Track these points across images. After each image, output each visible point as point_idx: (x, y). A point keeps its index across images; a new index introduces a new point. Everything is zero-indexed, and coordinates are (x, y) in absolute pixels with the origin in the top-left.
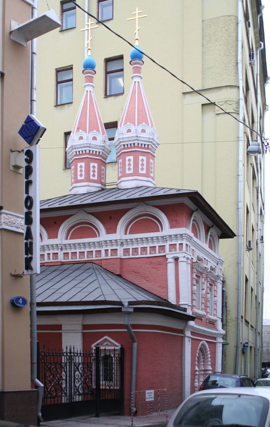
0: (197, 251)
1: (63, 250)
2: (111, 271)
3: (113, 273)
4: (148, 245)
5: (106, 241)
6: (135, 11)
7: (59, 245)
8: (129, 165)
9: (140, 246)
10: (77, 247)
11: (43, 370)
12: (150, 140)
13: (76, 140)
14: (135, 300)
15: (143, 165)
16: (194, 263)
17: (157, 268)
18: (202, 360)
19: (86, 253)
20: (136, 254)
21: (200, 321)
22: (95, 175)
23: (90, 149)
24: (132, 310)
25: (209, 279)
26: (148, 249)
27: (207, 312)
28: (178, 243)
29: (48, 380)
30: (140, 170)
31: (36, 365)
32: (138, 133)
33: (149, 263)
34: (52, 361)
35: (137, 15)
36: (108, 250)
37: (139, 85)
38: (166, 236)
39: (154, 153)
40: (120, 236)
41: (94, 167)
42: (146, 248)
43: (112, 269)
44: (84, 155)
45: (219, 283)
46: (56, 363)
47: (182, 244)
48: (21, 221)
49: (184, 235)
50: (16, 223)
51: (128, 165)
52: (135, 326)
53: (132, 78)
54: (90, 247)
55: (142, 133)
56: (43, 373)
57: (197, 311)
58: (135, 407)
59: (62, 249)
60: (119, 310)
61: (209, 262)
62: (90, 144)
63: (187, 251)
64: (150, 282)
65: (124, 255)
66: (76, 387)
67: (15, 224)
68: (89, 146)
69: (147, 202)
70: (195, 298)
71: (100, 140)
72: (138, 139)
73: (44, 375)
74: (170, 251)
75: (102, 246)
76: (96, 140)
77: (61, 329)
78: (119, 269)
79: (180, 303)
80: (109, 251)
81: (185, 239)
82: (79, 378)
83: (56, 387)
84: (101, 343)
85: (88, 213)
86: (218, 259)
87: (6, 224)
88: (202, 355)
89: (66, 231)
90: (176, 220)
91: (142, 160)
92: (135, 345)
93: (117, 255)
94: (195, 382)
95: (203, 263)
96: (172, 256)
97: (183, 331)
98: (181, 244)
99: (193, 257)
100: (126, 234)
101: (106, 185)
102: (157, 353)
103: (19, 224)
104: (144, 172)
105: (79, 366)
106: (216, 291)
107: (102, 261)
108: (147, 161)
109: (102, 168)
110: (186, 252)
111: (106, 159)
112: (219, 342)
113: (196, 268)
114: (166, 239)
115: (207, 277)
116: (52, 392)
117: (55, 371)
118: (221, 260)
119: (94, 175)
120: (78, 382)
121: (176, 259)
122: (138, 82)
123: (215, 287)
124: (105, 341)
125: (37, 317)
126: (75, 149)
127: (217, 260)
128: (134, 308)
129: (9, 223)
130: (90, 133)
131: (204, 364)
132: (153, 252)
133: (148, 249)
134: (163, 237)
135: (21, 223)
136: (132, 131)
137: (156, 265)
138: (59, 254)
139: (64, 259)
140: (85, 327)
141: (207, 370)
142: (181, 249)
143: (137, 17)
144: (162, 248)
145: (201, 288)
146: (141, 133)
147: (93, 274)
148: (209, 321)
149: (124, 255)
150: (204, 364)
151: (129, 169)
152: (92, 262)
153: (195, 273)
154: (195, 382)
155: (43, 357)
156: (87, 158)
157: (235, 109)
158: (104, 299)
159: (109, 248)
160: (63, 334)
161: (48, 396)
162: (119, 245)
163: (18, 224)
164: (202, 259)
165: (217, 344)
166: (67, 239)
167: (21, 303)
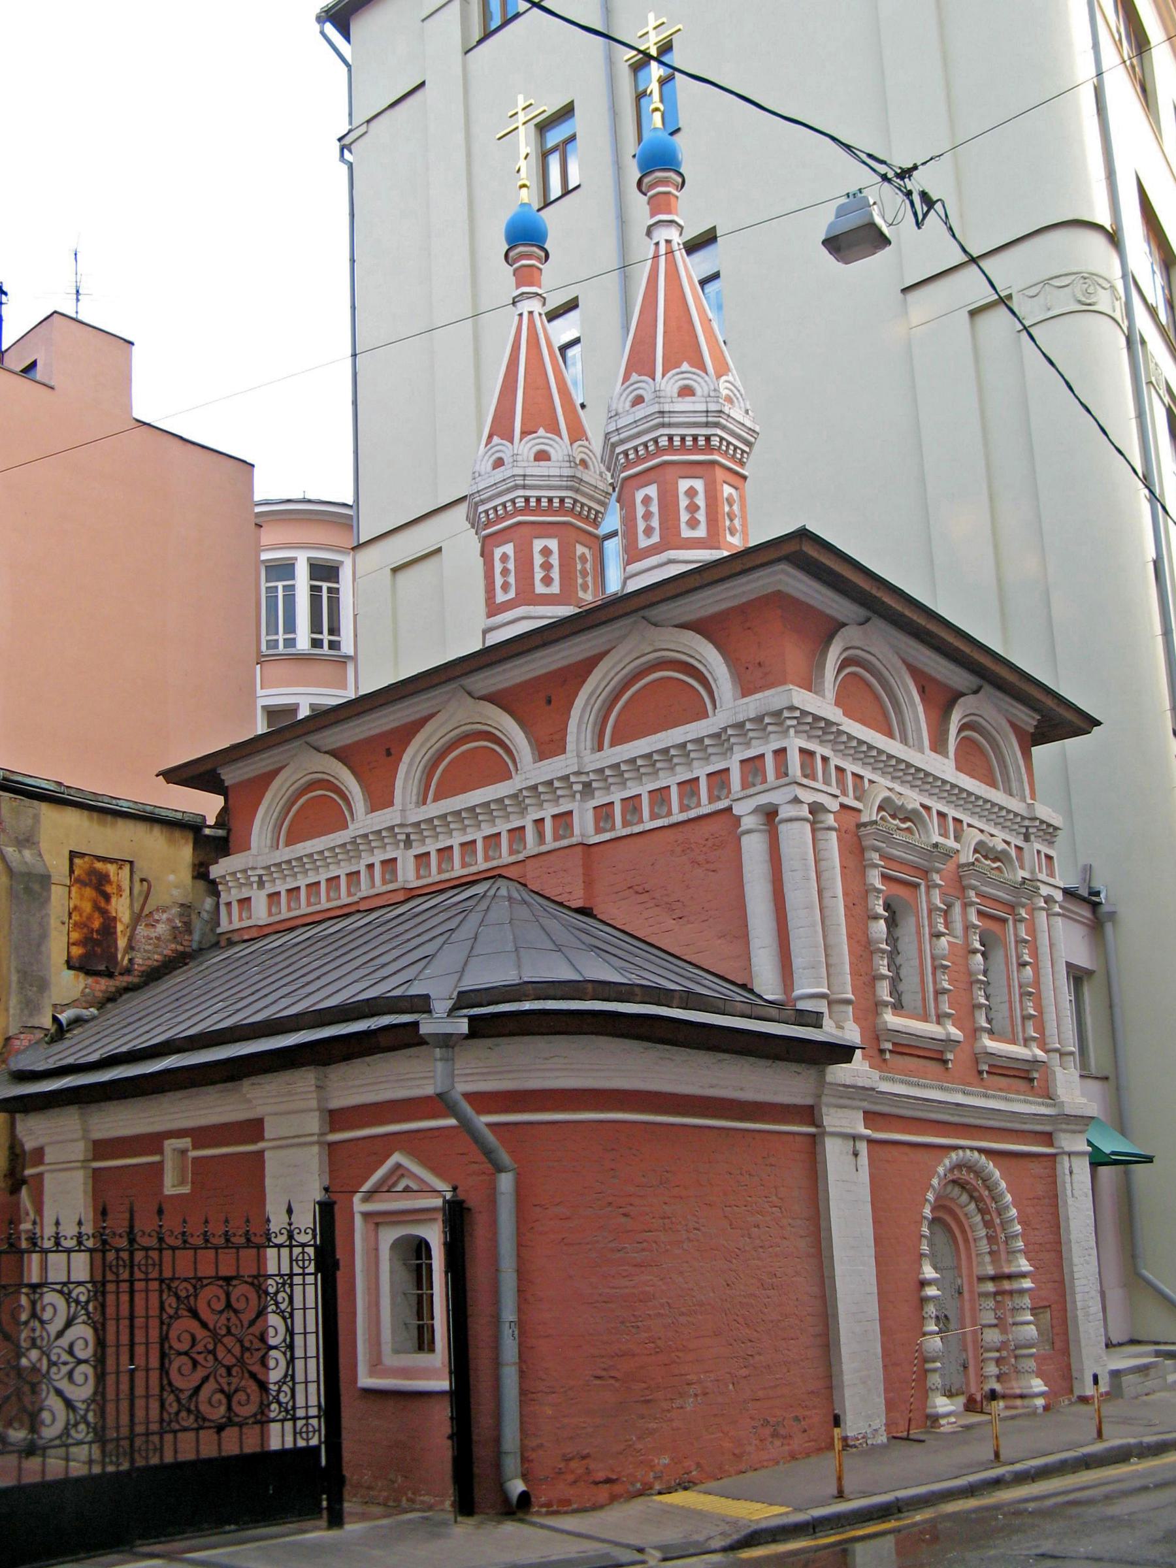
1: (414, 844)
2: (556, 899)
4: (670, 780)
5: (534, 788)
7: (397, 830)
9: (643, 789)
12: (710, 419)
13: (483, 473)
23: (528, 493)
24: (463, 1027)
25: (972, 893)
30: (683, 526)
32: (662, 400)
33: (678, 850)
35: (652, 34)
36: (542, 820)
38: (725, 729)
39: (741, 463)
40: (575, 760)
41: (546, 552)
43: (560, 890)
44: (512, 516)
47: (784, 750)
49: (786, 714)
52: (484, 1101)
53: (649, 233)
58: (525, 1477)
59: (408, 843)
61: (969, 825)
62: (524, 476)
64: (689, 922)
65: (599, 830)
66: (174, 1390)
68: (522, 482)
70: (946, 985)
72: (666, 420)
74: (744, 786)
76: (548, 459)
77: (260, 1137)
79: (798, 992)
80: (548, 824)
81: (792, 731)
86: (1023, 818)
91: (691, 492)
92: (506, 1182)
96: (752, 804)
98: (781, 753)
102: (625, 1215)
104: (701, 532)
108: (706, 491)
109: (578, 553)
111: (596, 523)
113: (876, 849)
119: (547, 581)
121: (770, 814)
124: (399, 1173)
128: (472, 1019)
130: (525, 439)
131: (995, 1248)
133: (674, 792)
136: (646, 399)
137: (704, 849)
139: (418, 877)
141: (1009, 1277)
142: (782, 771)
144: (719, 778)
145: (927, 929)
149: (599, 830)
152: (500, 876)
153: (876, 866)
156: (519, 524)
157: (1083, 299)
160: (267, 1155)
162: (578, 796)
164: (915, 811)
165: (1058, 1158)
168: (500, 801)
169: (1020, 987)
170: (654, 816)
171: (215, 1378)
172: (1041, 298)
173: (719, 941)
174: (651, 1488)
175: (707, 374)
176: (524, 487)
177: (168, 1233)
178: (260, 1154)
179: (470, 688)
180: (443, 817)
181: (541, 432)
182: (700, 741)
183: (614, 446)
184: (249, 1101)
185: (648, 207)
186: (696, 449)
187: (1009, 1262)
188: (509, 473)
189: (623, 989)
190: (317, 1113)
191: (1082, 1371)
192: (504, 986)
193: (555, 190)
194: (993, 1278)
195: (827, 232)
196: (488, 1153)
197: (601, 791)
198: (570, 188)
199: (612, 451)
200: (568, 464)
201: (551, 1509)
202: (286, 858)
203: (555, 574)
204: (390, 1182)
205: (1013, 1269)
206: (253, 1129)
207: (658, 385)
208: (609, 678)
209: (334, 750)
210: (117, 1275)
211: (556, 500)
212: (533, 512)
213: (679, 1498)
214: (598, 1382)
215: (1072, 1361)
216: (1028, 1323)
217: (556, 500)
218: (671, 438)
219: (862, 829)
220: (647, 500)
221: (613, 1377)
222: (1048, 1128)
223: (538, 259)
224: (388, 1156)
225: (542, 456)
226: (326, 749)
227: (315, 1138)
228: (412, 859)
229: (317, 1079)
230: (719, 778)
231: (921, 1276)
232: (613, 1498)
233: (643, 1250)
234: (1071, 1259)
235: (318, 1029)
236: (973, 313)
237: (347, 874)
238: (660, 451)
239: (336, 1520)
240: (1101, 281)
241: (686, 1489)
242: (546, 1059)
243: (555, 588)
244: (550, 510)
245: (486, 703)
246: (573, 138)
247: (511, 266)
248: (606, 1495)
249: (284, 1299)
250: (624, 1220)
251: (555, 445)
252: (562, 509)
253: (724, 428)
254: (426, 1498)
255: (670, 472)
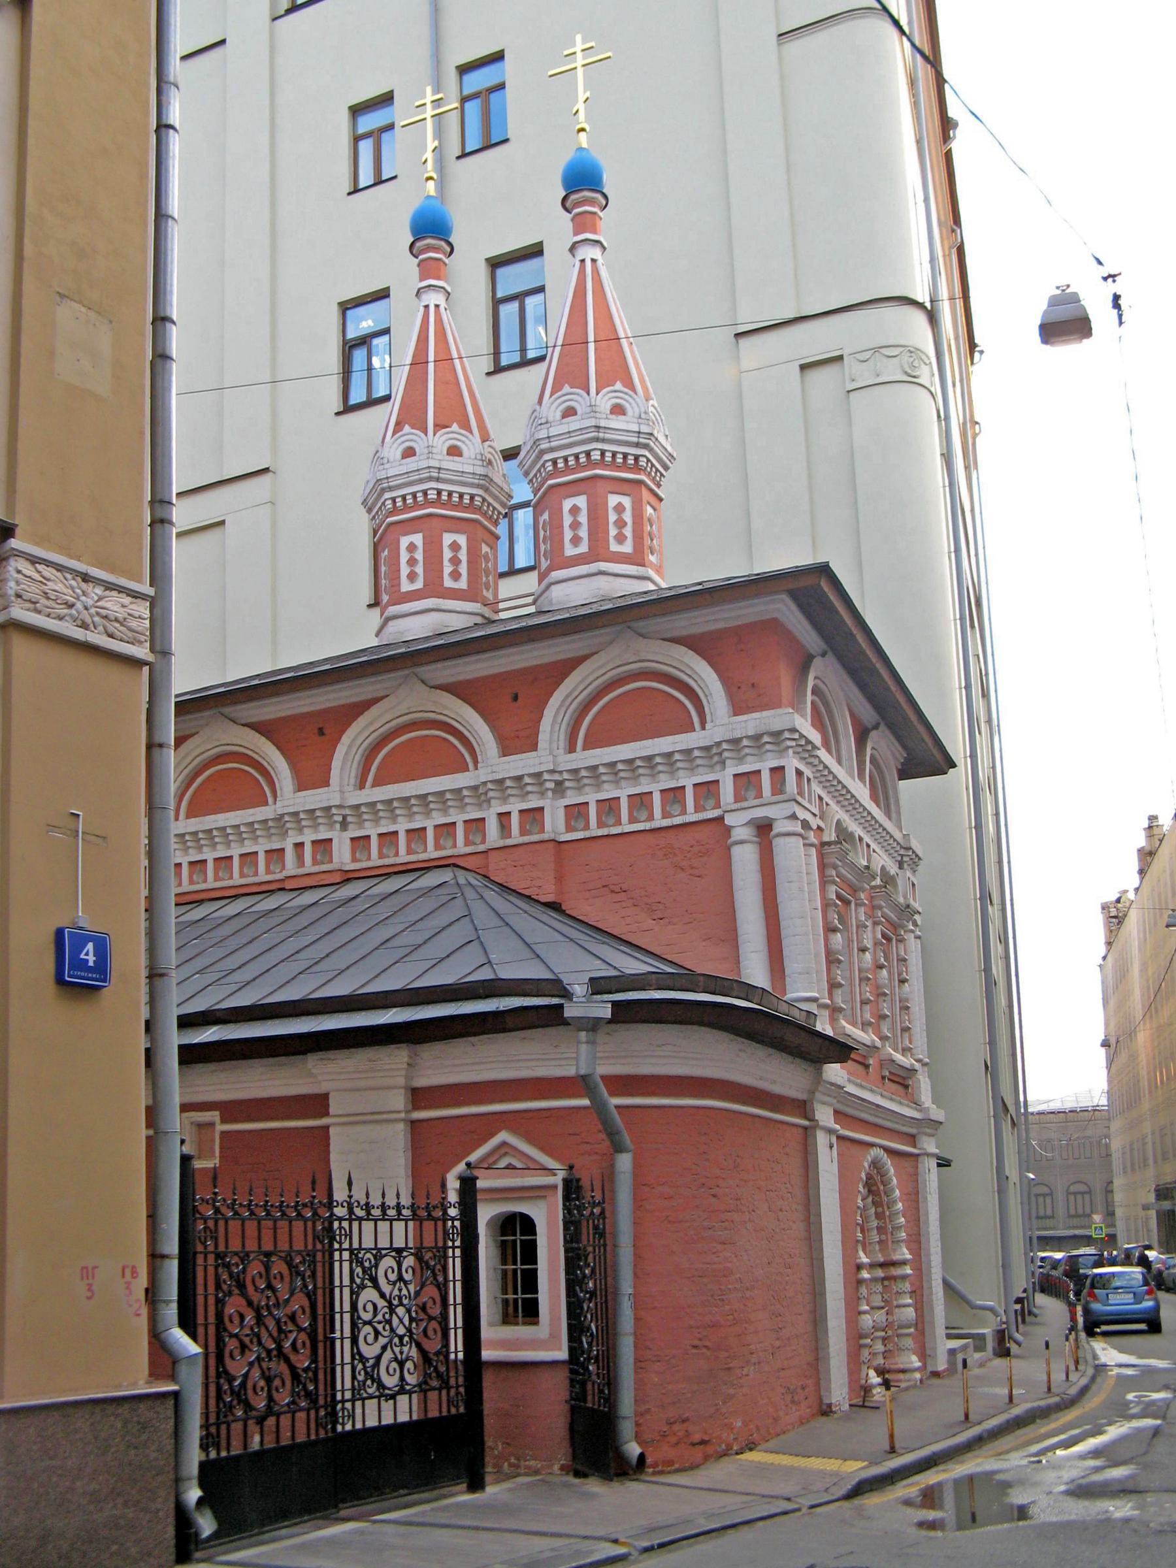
0: (834, 806)
1: (351, 826)
3: (529, 897)
4: (654, 786)
5: (500, 782)
6: (574, 45)
7: (334, 811)
8: (575, 525)
9: (624, 792)
10: (398, 812)
11: (211, 1289)
12: (641, 440)
13: (391, 459)
14: (614, 973)
15: (621, 524)
16: (829, 844)
17: (692, 868)
18: (875, 1224)
19: (430, 833)
20: (611, 821)
21: (860, 1068)
22: (460, 575)
24: (607, 1012)
26: (657, 799)
27: (883, 1038)
28: (765, 765)
29: (231, 1336)
30: (611, 540)
31: (172, 1268)
32: (598, 415)
34: (251, 1245)
35: (579, 55)
37: (596, 271)
38: (719, 744)
40: (550, 758)
41: (455, 547)
42: (648, 796)
44: (422, 507)
45: (912, 935)
46: (268, 1255)
48: (100, 599)
49: (787, 735)
50: (79, 606)
51: (570, 526)
52: (623, 1084)
54: (445, 811)
55: (614, 417)
56: (211, 1300)
57: (850, 1029)
58: (638, 1438)
59: (344, 825)
60: (552, 1017)
62: (440, 469)
63: (801, 793)
65: (569, 828)
66: (363, 1359)
67: (72, 606)
68: (436, 475)
69: (640, 625)
71: (473, 457)
72: (601, 435)
73: (217, 1315)
74: (738, 798)
75: (488, 801)
76: (460, 454)
78: (553, 881)
80: (515, 819)
81: (790, 751)
82: (379, 1317)
83: (269, 1369)
84: (488, 1163)
85: (432, 687)
87: (32, 606)
88: (873, 1202)
89: (358, 757)
90: (753, 685)
91: (619, 508)
92: (624, 1162)
93: (542, 830)
94: (860, 1313)
95: (857, 853)
97: (808, 1107)
98: (778, 771)
99: (822, 825)
100: (571, 749)
101: (502, 606)
102: (714, 1196)
103: (93, 611)
104: (627, 548)
105: (376, 1266)
106: (905, 960)
107: (487, 858)
108: (633, 509)
110: (799, 799)
112: (928, 1155)
114: (720, 754)
115: (873, 908)
116: (250, 1392)
117: (263, 1290)
118: (914, 852)
119: (456, 575)
120: (376, 1338)
121: (764, 828)
122: (594, 261)
123: (901, 946)
124: (503, 1151)
125: (179, 1035)
126: (391, 489)
127: (898, 848)
128: (615, 1004)
129: (43, 601)
130: (438, 434)
131: (883, 1237)
132: (676, 809)
133: (657, 799)
134: (707, 749)
135: (99, 604)
136: (579, 412)
137: (688, 855)
138: (335, 843)
139: (354, 860)
140: (419, 1097)
141: (894, 1264)
143: (580, 60)
144: (708, 789)
146: (610, 416)
147: (456, 900)
148: (890, 1072)
149: (569, 828)
150: (883, 1237)
151: (576, 541)
154: (860, 1313)
155: (211, 1224)
156: (430, 515)
158: (492, 977)
159: (515, 807)
161: (233, 1414)
162: (550, 794)
163: (86, 608)
165: (920, 1159)
166: (362, 786)
167: (91, 964)
168: (458, 791)
169: (900, 1002)
170: (632, 820)
171: (391, 1348)
172: (871, 362)
173: (704, 944)
174: (731, 1449)
175: (636, 394)
176: (438, 480)
177: (356, 1204)
178: (326, 1128)
179: (425, 676)
180: (389, 802)
181: (455, 427)
182: (688, 752)
183: (543, 452)
184: (312, 1075)
185: (571, 224)
186: (624, 467)
187: (894, 1250)
188: (424, 464)
189: (726, 983)
190: (402, 1091)
191: (935, 1349)
192: (634, 975)
193: (365, 179)
194: (882, 1265)
195: (1043, 316)
196: (612, 1133)
197: (573, 791)
198: (384, 178)
199: (539, 457)
200: (480, 463)
201: (657, 1469)
202: (193, 829)
203: (463, 569)
204: (491, 1160)
205: (897, 1257)
206: (318, 1104)
207: (593, 400)
208: (587, 682)
209: (259, 723)
210: (206, 1247)
211: (467, 497)
212: (443, 505)
213: (749, 1456)
214: (694, 1351)
215: (927, 1340)
216: (908, 1305)
217: (467, 497)
218: (603, 453)
219: (826, 847)
220: (575, 510)
221: (706, 1347)
222: (913, 1131)
223: (444, 254)
224: (492, 1135)
225: (454, 451)
226: (243, 722)
227: (403, 1115)
228: (348, 841)
229: (410, 1057)
230: (708, 789)
231: (858, 1261)
232: (707, 1458)
233: (726, 1229)
234: (929, 1250)
235: (419, 1008)
236: (803, 367)
237: (266, 852)
238: (591, 464)
239: (476, 1484)
240: (924, 357)
241: (751, 1450)
242: (658, 1046)
243: (463, 584)
244: (459, 506)
245: (444, 693)
246: (390, 127)
247: (416, 257)
248: (700, 1455)
249: (407, 1272)
250: (714, 1200)
251: (467, 442)
252: (471, 507)
253: (651, 450)
254: (532, 1463)
255: (601, 486)
